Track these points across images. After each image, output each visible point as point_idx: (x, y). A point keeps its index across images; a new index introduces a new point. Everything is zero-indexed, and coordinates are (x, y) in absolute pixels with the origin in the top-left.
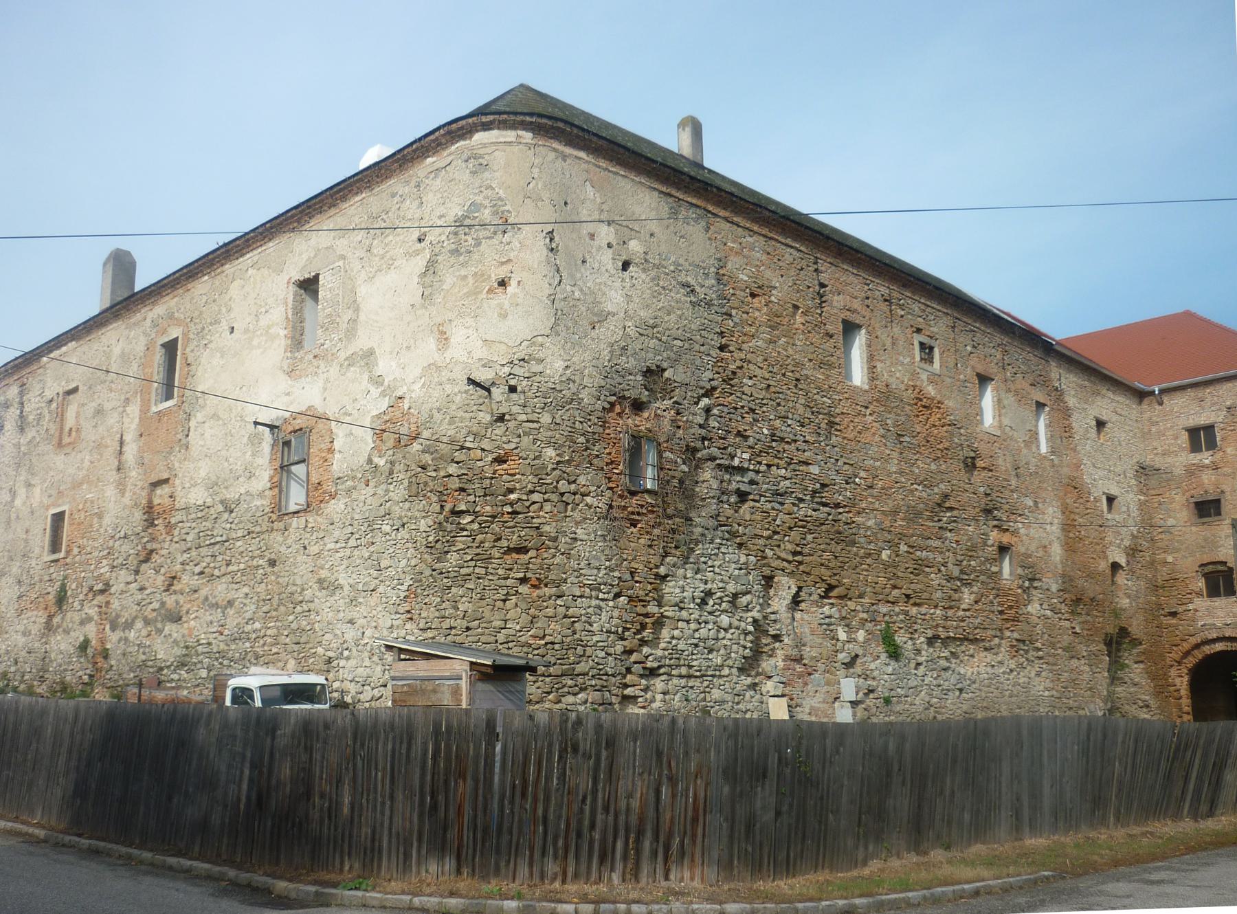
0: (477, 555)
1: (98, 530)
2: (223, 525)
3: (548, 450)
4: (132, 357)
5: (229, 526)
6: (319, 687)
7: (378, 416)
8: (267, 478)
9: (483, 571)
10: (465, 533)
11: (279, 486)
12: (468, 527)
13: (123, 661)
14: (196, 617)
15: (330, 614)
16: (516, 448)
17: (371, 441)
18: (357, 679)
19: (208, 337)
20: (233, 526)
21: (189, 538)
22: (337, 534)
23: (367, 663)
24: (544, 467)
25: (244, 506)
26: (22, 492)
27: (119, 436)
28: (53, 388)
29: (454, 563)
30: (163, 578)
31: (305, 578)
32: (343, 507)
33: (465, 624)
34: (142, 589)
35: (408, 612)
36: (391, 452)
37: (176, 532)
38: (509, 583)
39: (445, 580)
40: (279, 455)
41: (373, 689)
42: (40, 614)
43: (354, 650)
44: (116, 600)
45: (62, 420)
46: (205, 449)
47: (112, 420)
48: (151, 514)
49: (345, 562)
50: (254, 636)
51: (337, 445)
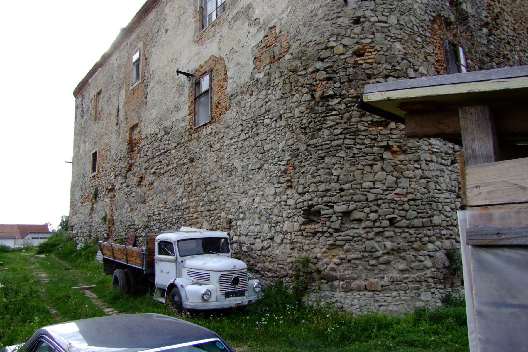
0: (345, 129)
1: (109, 158)
2: (165, 142)
3: (396, 43)
4: (122, 65)
5: (167, 142)
6: (223, 240)
7: (257, 46)
8: (187, 108)
9: (352, 142)
10: (334, 113)
11: (193, 112)
12: (336, 107)
13: (120, 226)
14: (153, 199)
15: (229, 189)
16: (372, 42)
17: (252, 64)
18: (250, 234)
19: (155, 40)
20: (170, 142)
21: (148, 154)
22: (232, 133)
23: (257, 222)
24: (394, 56)
25: (175, 129)
26: (82, 146)
27: (117, 107)
28: (94, 92)
29: (326, 137)
30: (137, 178)
31: (212, 166)
32: (235, 114)
33: (338, 187)
34: (128, 186)
35: (288, 181)
36: (268, 67)
37: (142, 152)
38: (375, 149)
39: (320, 152)
40: (193, 92)
41: (262, 241)
42: (89, 204)
43: (247, 213)
44: (117, 194)
45: (96, 107)
46: (155, 102)
47: (114, 100)
48: (132, 145)
49: (238, 151)
50: (183, 207)
51: (229, 74)
